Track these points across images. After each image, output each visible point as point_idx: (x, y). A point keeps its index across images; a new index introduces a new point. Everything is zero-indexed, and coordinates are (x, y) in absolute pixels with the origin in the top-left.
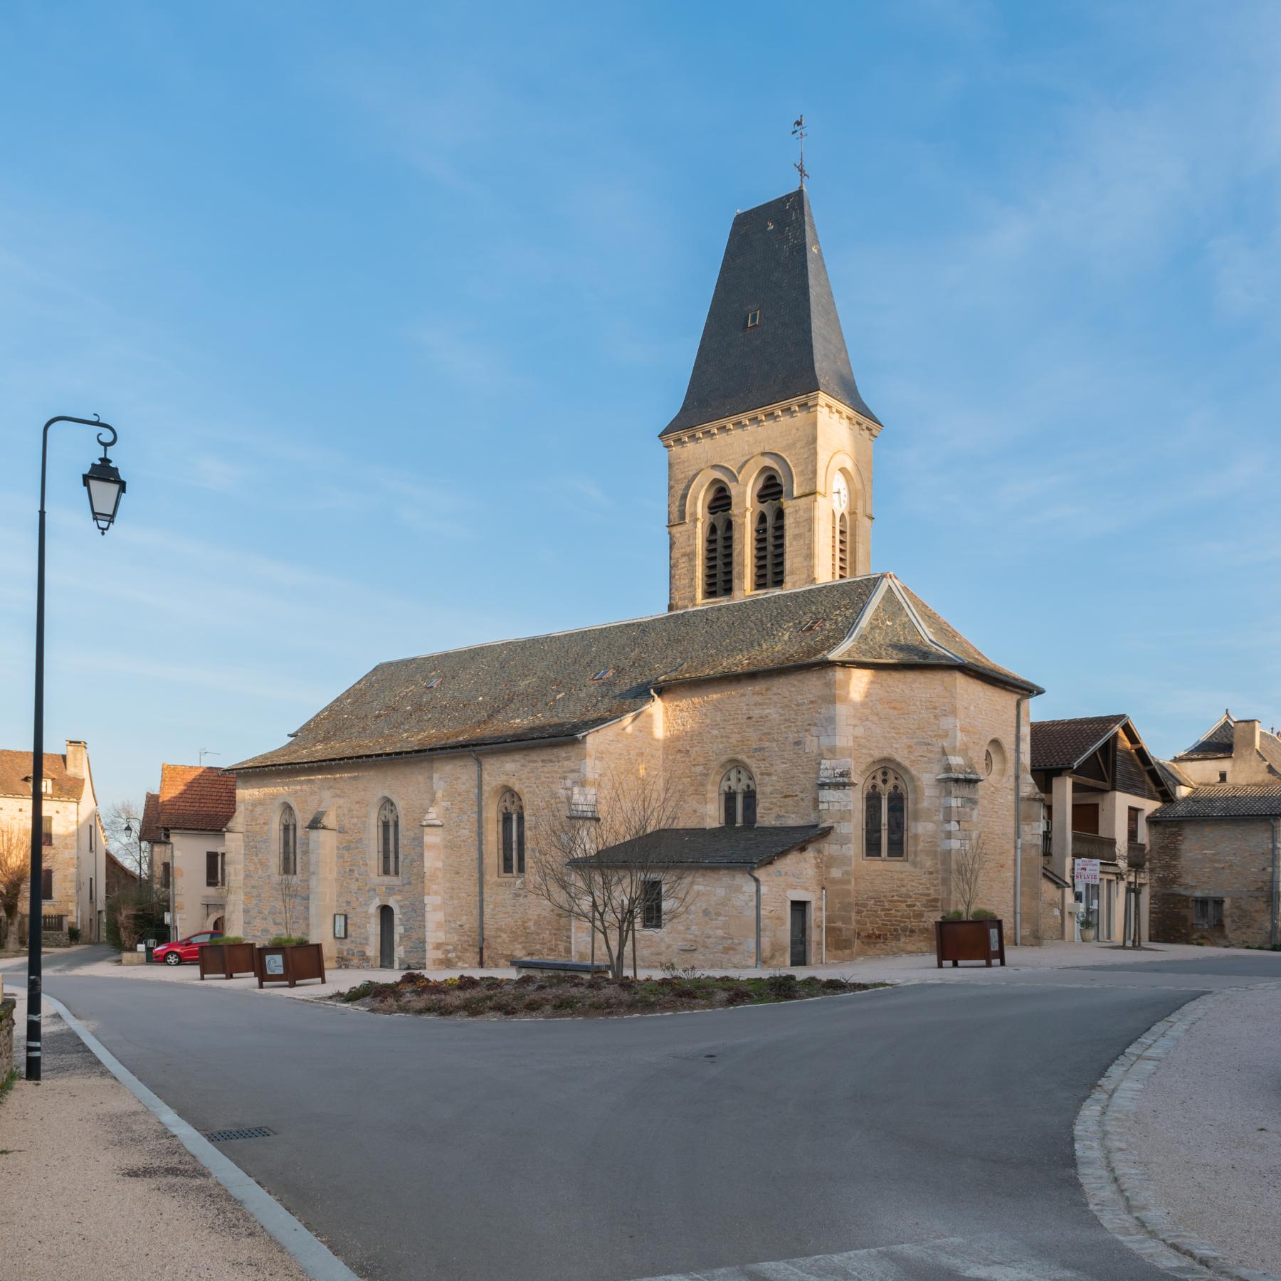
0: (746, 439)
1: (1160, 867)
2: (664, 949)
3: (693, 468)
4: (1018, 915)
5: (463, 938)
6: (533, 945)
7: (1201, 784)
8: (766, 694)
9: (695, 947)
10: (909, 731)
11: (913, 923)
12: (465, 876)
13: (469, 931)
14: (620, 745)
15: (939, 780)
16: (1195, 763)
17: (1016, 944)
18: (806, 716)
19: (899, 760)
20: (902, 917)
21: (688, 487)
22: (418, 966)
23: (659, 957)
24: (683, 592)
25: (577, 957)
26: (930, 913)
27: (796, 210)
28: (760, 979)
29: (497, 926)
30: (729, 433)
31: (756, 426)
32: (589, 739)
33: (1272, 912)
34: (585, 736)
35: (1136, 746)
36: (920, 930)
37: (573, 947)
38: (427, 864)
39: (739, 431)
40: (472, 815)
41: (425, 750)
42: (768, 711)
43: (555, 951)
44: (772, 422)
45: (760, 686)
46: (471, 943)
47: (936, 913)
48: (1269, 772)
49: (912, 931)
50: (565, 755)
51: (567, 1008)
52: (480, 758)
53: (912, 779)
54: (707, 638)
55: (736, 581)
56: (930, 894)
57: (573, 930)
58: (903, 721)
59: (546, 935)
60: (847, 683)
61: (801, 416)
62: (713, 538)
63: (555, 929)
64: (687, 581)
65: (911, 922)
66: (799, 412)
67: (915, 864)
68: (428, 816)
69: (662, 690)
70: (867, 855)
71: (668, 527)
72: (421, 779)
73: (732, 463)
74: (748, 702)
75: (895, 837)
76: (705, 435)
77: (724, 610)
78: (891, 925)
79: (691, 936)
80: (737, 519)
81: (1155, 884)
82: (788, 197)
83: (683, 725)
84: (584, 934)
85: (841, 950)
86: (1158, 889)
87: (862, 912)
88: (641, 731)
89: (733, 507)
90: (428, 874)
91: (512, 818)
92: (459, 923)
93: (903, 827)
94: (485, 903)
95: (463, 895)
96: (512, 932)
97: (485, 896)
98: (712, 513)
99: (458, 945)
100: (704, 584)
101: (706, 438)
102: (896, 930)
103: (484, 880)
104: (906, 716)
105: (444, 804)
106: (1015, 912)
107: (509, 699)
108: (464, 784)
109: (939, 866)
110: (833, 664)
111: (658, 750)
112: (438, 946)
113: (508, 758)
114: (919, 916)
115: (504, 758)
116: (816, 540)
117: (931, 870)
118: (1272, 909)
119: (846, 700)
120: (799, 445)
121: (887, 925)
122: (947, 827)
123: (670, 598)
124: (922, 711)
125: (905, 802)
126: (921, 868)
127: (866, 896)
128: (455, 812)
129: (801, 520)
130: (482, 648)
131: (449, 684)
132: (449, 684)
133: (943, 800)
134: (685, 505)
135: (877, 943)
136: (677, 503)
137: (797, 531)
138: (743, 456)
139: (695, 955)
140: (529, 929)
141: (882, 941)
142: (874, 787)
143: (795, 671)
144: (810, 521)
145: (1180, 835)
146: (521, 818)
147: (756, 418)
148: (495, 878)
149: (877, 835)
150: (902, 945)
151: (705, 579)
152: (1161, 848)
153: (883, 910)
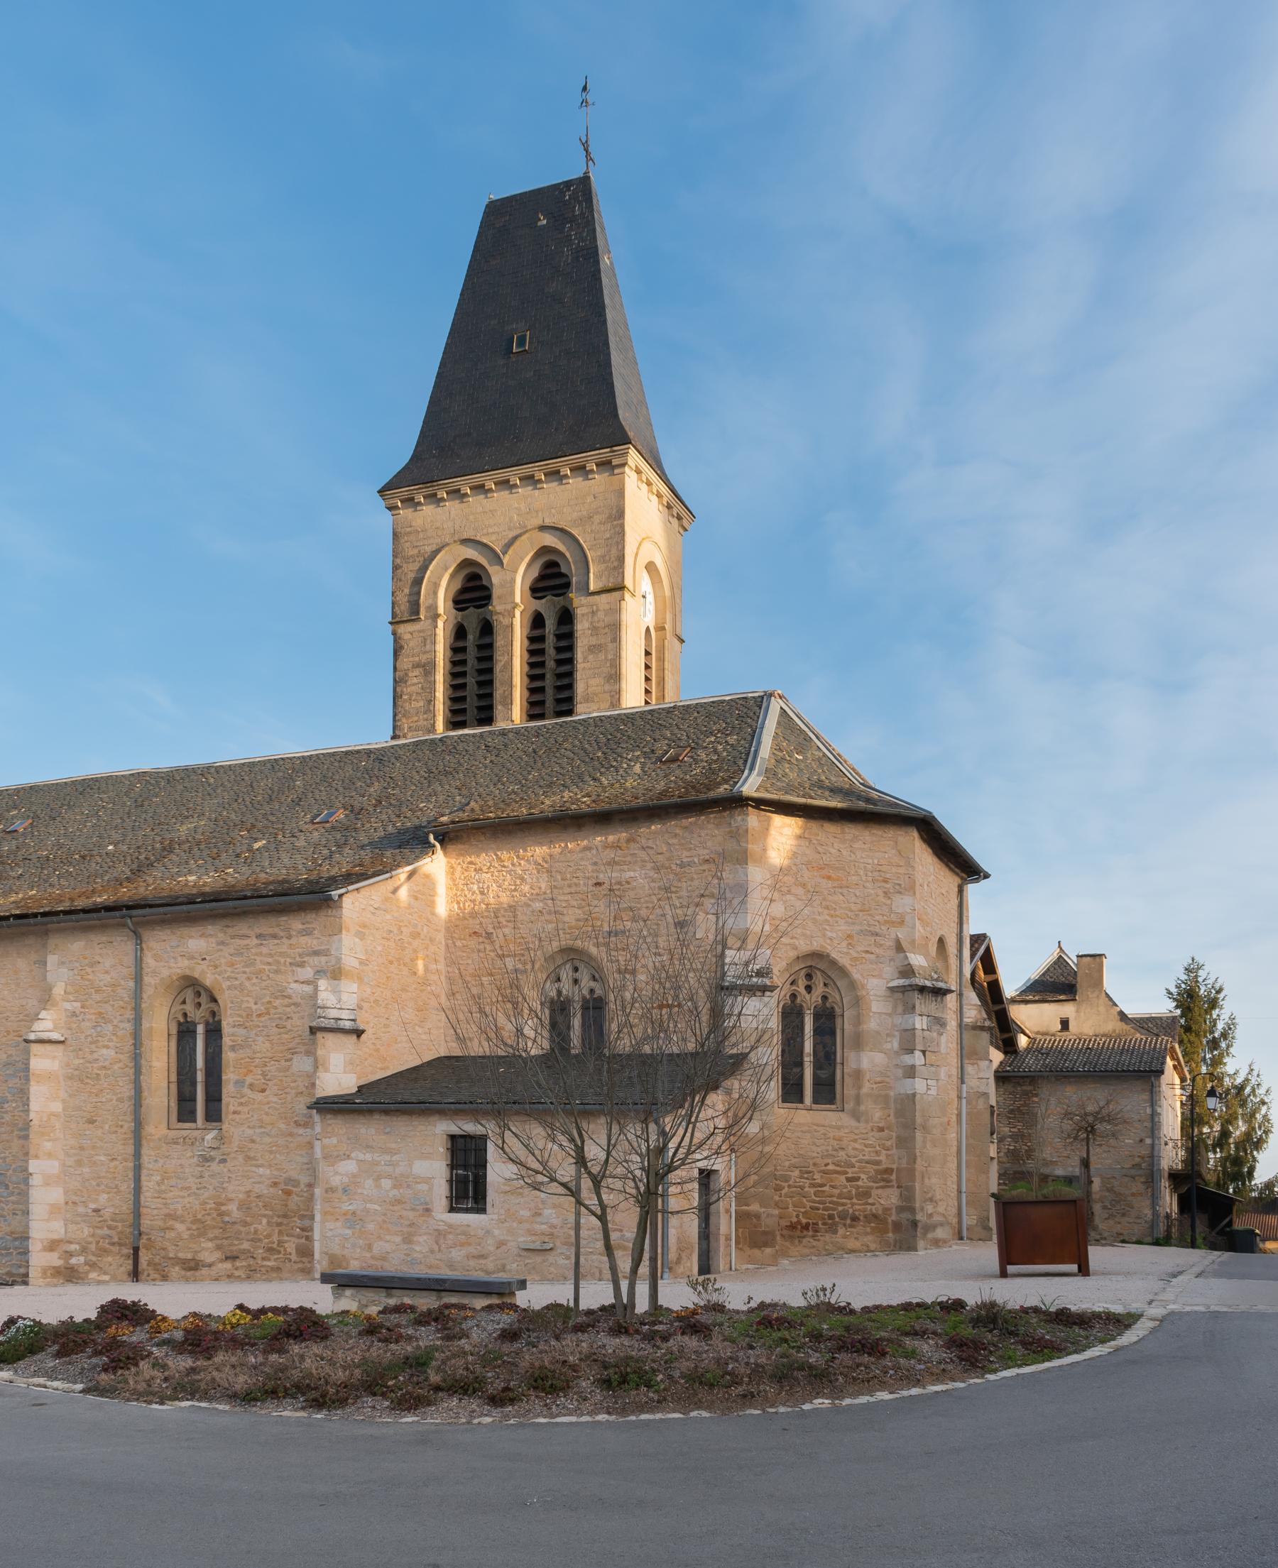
0: (516, 505)
1: (1010, 1137)
2: (492, 1249)
3: (431, 541)
4: (964, 1196)
5: (99, 1232)
6: (236, 1242)
7: (1038, 1033)
8: (628, 848)
9: (551, 1245)
10: (849, 914)
11: (857, 1207)
12: (107, 1127)
13: (112, 1220)
14: (388, 917)
15: (892, 989)
16: (1030, 1006)
17: (961, 1238)
18: (696, 883)
19: (834, 955)
20: (840, 1196)
21: (424, 568)
22: (10, 1280)
23: (483, 1262)
24: (416, 718)
25: (325, 1263)
26: (880, 1191)
27: (580, 203)
28: (958, 1305)
29: (167, 1211)
30: (489, 495)
31: (530, 488)
32: (347, 902)
33: (1153, 1194)
34: (341, 896)
35: (991, 978)
36: (865, 1217)
37: (317, 1246)
38: (35, 1106)
39: (505, 494)
40: (122, 1025)
41: (35, 915)
42: (632, 874)
43: (279, 1252)
44: (555, 484)
45: (616, 836)
46: (116, 1240)
47: (889, 1191)
48: (1121, 1020)
49: (855, 1219)
50: (300, 926)
51: (637, 1387)
52: (140, 930)
53: (852, 985)
54: (496, 770)
55: (499, 707)
56: (881, 1161)
57: (318, 1217)
58: (841, 897)
59: (262, 1226)
60: (766, 830)
61: (600, 480)
62: (460, 644)
63: (279, 1217)
64: (421, 704)
65: (853, 1204)
66: (598, 473)
67: (856, 1116)
68: (38, 1026)
69: (447, 837)
70: (784, 1101)
71: (390, 623)
72: (22, 964)
73: (494, 538)
74: (595, 860)
75: (823, 1074)
76: (451, 496)
77: (511, 735)
78: (824, 1209)
79: (544, 1227)
80: (501, 618)
81: (1005, 1159)
82: (568, 184)
83: (482, 893)
84: (339, 1224)
85: (759, 1247)
86: (1008, 1165)
87: (782, 1188)
88: (416, 899)
89: (495, 601)
90: (35, 1122)
91: (195, 1032)
92: (93, 1206)
93: (835, 1059)
94: (144, 1172)
95: (103, 1158)
96: (195, 1221)
97: (145, 1159)
98: (458, 609)
99: (90, 1243)
100: (447, 710)
101: (453, 500)
102: (831, 1217)
103: (144, 1133)
104: (845, 891)
105: (68, 1006)
106: (960, 1192)
107: (164, 849)
108: (107, 972)
109: (892, 1119)
110: (740, 802)
111: (439, 931)
112: (52, 1246)
113: (195, 930)
114: (865, 1194)
115: (185, 931)
116: (623, 654)
117: (880, 1125)
118: (1153, 1190)
119: (762, 859)
120: (597, 519)
121: (818, 1209)
122: (908, 1060)
123: (395, 728)
124: (868, 885)
125: (838, 1021)
126: (867, 1122)
127: (787, 1164)
128: (89, 1020)
129: (601, 624)
130: (96, 780)
131: (46, 827)
132: (46, 827)
133: (898, 1020)
134: (419, 593)
135: (804, 1237)
136: (407, 591)
137: (594, 641)
138: (510, 529)
139: (551, 1258)
140: (228, 1215)
141: (811, 1233)
142: (793, 996)
143: (677, 813)
144: (615, 629)
145: (1036, 1095)
146: (214, 1032)
147: (532, 477)
148: (163, 1130)
149: (796, 1070)
150: (840, 1240)
151: (448, 703)
152: (1011, 1111)
153: (813, 1185)
